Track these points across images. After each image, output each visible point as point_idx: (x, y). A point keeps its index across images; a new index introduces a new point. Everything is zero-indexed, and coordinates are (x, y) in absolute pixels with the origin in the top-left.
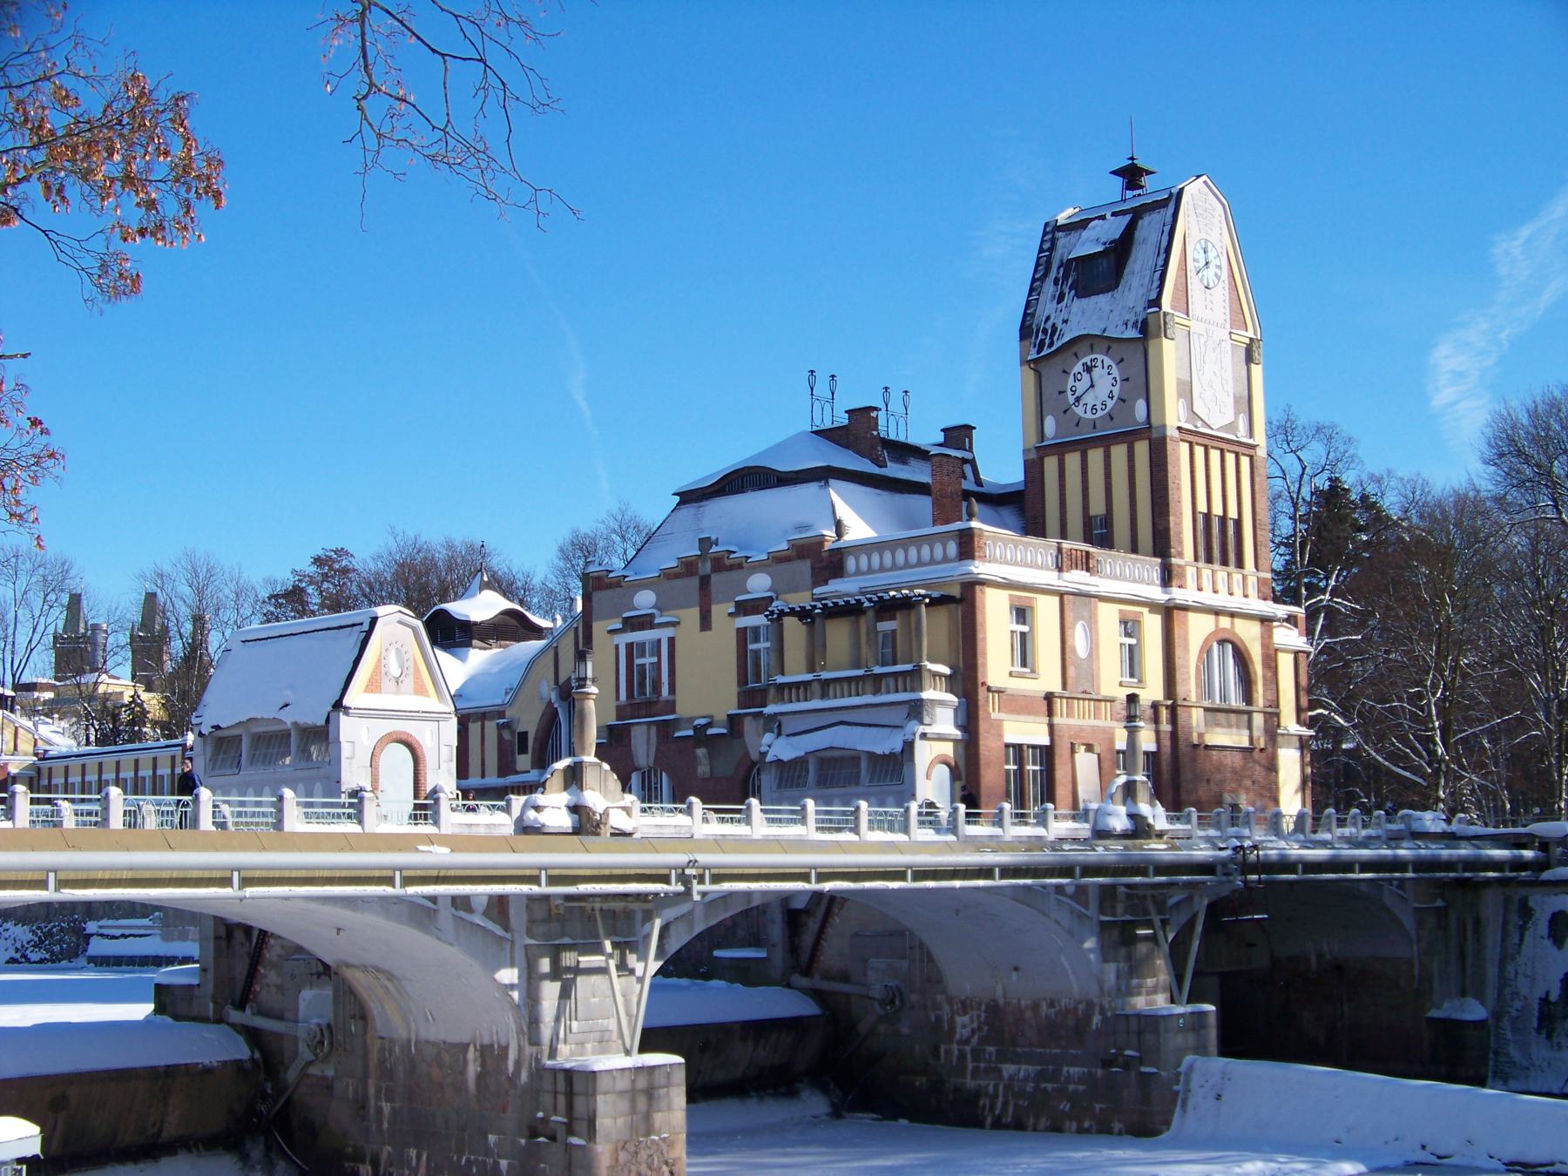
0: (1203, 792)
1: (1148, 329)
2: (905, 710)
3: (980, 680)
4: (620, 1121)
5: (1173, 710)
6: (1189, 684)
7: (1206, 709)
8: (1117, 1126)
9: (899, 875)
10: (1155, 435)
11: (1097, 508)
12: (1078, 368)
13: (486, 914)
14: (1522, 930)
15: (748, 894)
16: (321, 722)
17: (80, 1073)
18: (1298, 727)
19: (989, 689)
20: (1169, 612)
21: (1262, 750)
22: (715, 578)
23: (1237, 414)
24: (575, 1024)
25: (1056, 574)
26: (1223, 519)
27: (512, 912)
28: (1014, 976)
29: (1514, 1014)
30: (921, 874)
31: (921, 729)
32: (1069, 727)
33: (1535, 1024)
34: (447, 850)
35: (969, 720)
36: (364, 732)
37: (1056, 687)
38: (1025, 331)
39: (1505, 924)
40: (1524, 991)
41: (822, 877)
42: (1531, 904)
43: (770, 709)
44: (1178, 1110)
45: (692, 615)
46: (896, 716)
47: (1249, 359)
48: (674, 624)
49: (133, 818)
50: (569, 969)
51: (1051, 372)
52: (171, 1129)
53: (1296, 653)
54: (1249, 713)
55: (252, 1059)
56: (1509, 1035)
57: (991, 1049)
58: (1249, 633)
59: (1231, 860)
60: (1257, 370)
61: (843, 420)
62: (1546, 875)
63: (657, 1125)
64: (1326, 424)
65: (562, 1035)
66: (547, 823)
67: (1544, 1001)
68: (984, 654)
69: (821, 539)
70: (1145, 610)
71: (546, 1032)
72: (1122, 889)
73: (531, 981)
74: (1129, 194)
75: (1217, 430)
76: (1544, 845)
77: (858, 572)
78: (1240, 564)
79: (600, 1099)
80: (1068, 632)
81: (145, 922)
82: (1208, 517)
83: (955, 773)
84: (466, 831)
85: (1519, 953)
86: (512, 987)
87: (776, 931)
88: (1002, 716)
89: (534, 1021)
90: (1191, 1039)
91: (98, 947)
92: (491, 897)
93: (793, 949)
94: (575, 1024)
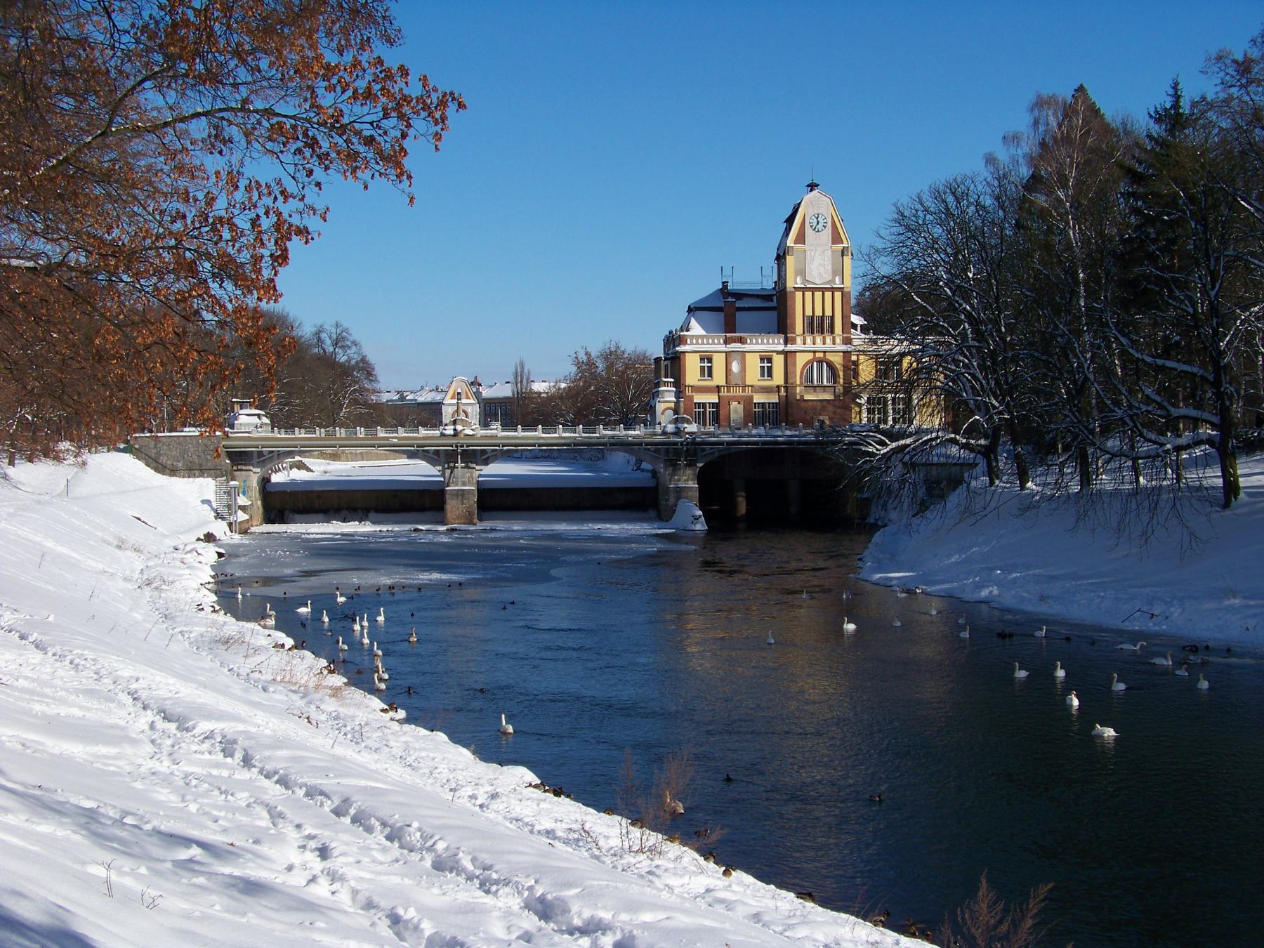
5: (786, 387)
13: (433, 454)
17: (424, 491)
35: (679, 394)
60: (847, 260)
70: (774, 354)
78: (832, 332)
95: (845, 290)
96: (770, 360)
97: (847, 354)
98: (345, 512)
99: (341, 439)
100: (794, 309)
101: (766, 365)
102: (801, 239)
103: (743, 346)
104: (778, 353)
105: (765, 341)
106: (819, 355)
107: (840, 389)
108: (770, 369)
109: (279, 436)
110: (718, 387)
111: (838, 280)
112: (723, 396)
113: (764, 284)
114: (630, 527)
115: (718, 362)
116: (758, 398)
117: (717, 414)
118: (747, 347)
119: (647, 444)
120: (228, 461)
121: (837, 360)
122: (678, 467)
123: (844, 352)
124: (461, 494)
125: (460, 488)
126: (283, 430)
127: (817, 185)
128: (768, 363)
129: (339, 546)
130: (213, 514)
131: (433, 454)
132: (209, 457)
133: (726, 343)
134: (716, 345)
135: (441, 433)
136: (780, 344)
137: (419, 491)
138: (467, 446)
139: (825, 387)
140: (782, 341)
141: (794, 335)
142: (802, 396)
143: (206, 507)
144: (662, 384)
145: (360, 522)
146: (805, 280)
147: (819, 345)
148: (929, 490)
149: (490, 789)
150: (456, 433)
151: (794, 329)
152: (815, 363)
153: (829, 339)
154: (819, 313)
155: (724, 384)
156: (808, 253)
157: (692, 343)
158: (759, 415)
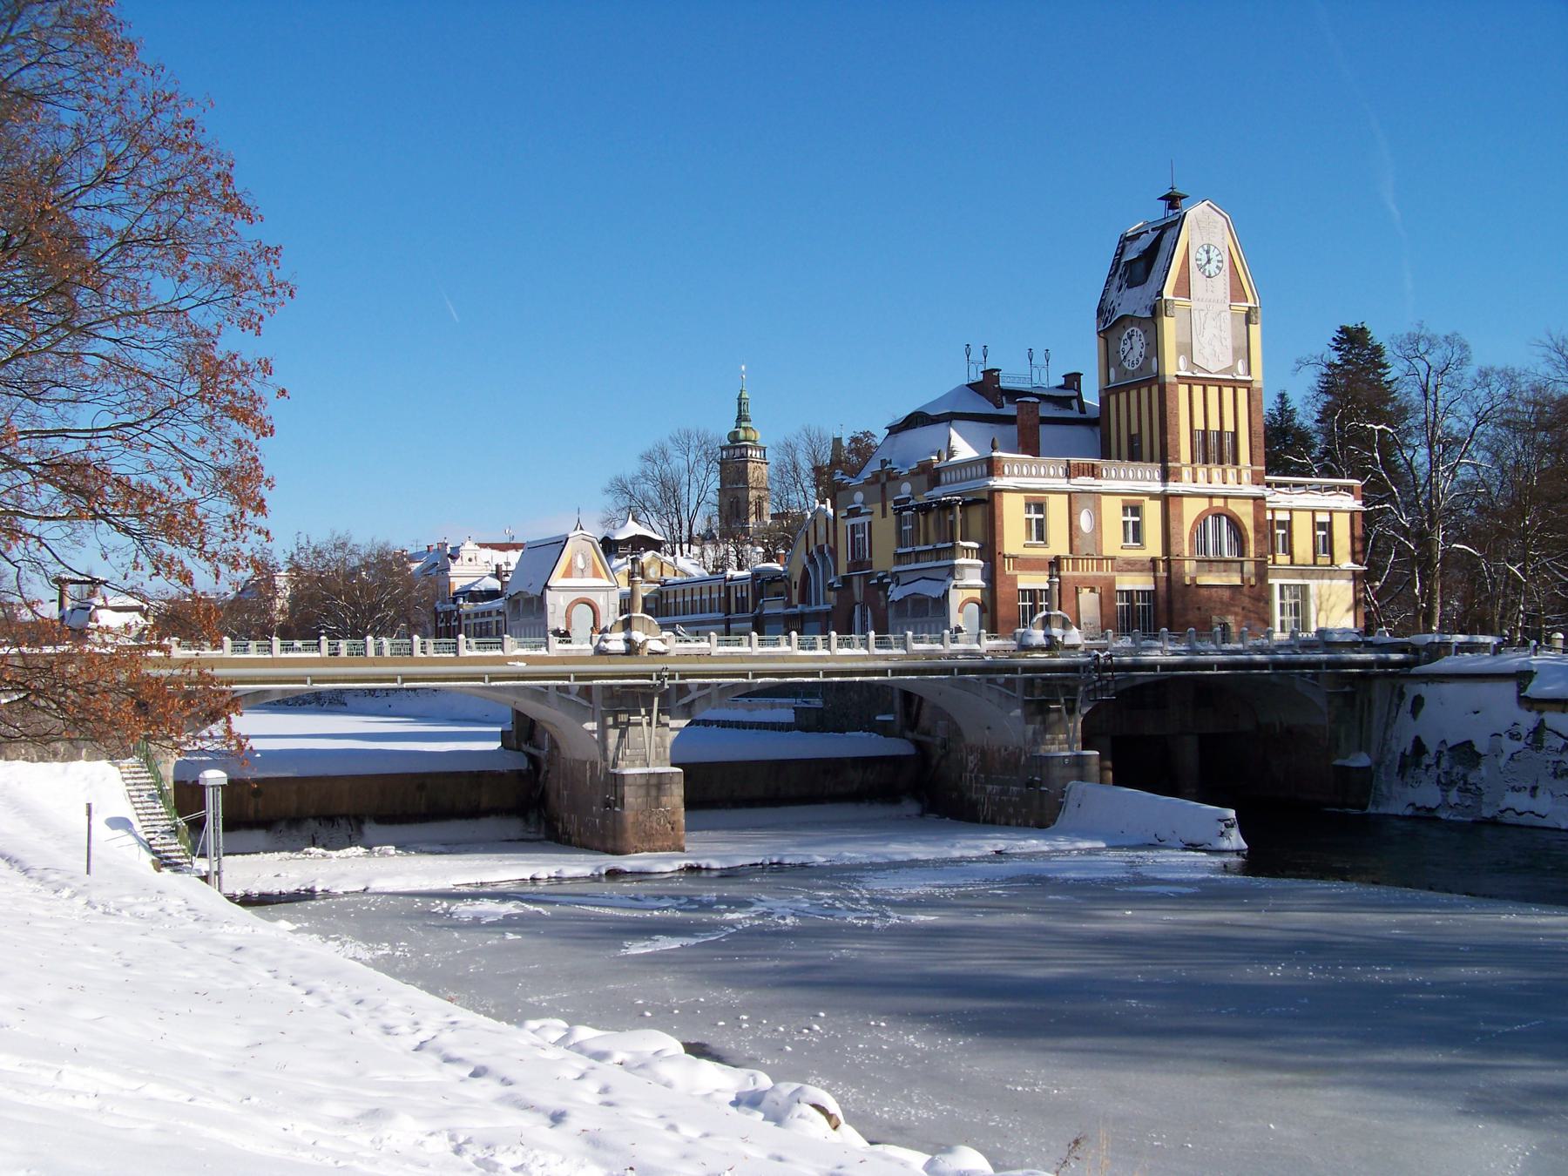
0: (1192, 616)
1: (1157, 311)
2: (947, 571)
4: (639, 800)
5: (1168, 563)
7: (1197, 561)
8: (1032, 822)
9: (815, 674)
10: (1160, 381)
11: (1134, 430)
12: (1125, 336)
13: (578, 695)
14: (1398, 706)
16: (539, 594)
18: (1352, 564)
19: (1004, 556)
21: (1251, 586)
22: (888, 485)
23: (1235, 361)
24: (628, 751)
25: (1066, 480)
26: (1221, 433)
28: (987, 732)
29: (1388, 763)
30: (828, 674)
31: (954, 582)
32: (1074, 577)
33: (1397, 770)
34: (524, 664)
35: (991, 575)
36: (562, 598)
37: (1063, 550)
38: (1100, 312)
39: (1391, 702)
40: (1394, 748)
41: (756, 676)
42: (1405, 690)
44: (1061, 813)
45: (878, 507)
46: (942, 574)
47: (1248, 321)
48: (871, 513)
49: (379, 651)
50: (623, 723)
51: (1112, 336)
52: (485, 802)
53: (1352, 513)
54: (1242, 562)
55: (528, 770)
56: (1383, 777)
57: (982, 776)
58: (1245, 512)
59: (1090, 663)
60: (1255, 330)
61: (981, 377)
62: (1415, 670)
63: (663, 803)
64: (411, 551)
65: (620, 756)
66: (610, 648)
67: (1403, 754)
69: (931, 462)
70: (1146, 499)
71: (611, 755)
72: (1039, 680)
73: (603, 729)
74: (1171, 212)
75: (1216, 373)
76: (1416, 649)
77: (947, 483)
78: (1236, 462)
80: (1074, 517)
82: (1205, 432)
83: (983, 608)
84: (565, 654)
85: (1395, 722)
86: (593, 732)
87: (897, 704)
88: (1017, 572)
89: (605, 749)
90: (1074, 772)
92: (581, 686)
93: (907, 714)
94: (628, 751)
95: (1255, 385)
96: (1136, 510)
98: (313, 825)
99: (421, 662)
100: (1177, 415)
101: (1130, 519)
102: (1184, 288)
103: (1097, 482)
104: (1153, 496)
106: (1218, 503)
107: (1249, 567)
111: (1241, 367)
112: (1067, 578)
113: (1036, 380)
115: (1057, 508)
118: (1104, 485)
119: (1026, 669)
122: (1053, 717)
123: (1255, 499)
124: (656, 784)
129: (1196, 931)
131: (578, 695)
133: (1068, 475)
139: (1226, 561)
141: (1178, 465)
142: (1193, 579)
144: (959, 550)
146: (1192, 364)
147: (1217, 486)
150: (632, 649)
151: (1178, 452)
156: (1195, 315)
157: (1011, 475)
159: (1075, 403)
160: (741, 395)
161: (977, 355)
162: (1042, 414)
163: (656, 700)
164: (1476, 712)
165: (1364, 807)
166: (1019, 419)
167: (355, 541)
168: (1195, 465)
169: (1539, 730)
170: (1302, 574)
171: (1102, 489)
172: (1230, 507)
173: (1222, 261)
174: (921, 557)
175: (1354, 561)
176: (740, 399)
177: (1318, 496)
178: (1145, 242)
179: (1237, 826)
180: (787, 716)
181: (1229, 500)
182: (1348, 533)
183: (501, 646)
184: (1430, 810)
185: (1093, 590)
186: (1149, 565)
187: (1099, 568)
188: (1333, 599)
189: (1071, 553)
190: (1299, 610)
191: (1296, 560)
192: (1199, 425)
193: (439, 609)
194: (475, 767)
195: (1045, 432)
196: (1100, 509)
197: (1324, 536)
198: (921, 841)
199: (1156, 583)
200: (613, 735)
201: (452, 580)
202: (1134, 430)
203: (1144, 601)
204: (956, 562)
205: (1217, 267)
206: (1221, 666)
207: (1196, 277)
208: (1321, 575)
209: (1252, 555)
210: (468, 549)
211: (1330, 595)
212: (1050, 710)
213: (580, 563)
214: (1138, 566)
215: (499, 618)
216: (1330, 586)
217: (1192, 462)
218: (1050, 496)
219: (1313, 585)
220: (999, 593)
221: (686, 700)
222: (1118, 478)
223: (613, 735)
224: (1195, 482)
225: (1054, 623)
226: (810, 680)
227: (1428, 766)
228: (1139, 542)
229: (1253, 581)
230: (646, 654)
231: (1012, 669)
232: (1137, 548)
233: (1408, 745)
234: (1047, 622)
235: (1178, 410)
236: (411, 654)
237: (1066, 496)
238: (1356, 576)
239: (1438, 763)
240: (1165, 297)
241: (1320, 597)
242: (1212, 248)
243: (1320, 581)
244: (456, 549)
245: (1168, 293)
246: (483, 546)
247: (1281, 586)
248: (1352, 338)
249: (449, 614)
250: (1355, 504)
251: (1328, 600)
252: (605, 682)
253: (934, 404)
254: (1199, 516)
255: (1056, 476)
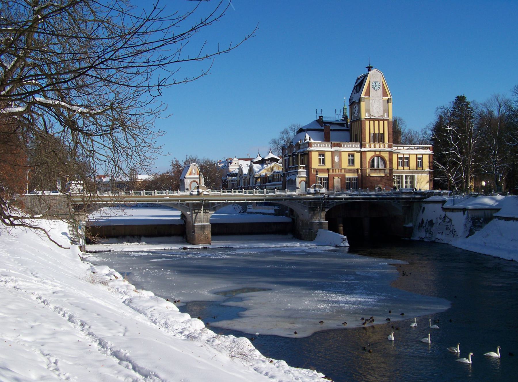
3: (310, 167)
5: (361, 170)
6: (366, 165)
11: (356, 134)
13: (186, 205)
15: (145, 203)
17: (171, 225)
19: (312, 169)
20: (361, 152)
23: (384, 114)
26: (379, 134)
27: (190, 205)
30: (248, 200)
31: (298, 176)
32: (333, 174)
35: (308, 173)
36: (188, 181)
38: (350, 100)
41: (228, 201)
43: (288, 172)
47: (388, 102)
50: (196, 212)
53: (430, 155)
54: (385, 170)
60: (390, 105)
67: (419, 223)
68: (311, 163)
70: (355, 152)
71: (194, 220)
75: (378, 117)
78: (384, 142)
79: (196, 228)
80: (333, 158)
81: (251, 206)
86: (190, 214)
91: (248, 210)
94: (198, 219)
95: (390, 120)
96: (353, 156)
97: (390, 153)
98: (128, 237)
100: (365, 129)
101: (351, 158)
102: (368, 93)
103: (340, 148)
105: (351, 146)
107: (387, 171)
108: (353, 160)
109: (245, 195)
110: (328, 170)
111: (386, 115)
113: (337, 118)
114: (309, 245)
115: (328, 156)
116: (348, 175)
117: (327, 182)
118: (342, 149)
119: (304, 199)
120: (73, 210)
121: (386, 156)
122: (316, 212)
123: (389, 152)
124: (203, 227)
125: (202, 224)
126: (247, 191)
127: (372, 67)
128: (352, 157)
130: (69, 241)
131: (186, 205)
132: (62, 207)
134: (326, 147)
135: (190, 194)
136: (358, 147)
137: (169, 225)
138: (208, 201)
140: (359, 146)
141: (365, 143)
142: (369, 175)
143: (65, 237)
145: (139, 243)
147: (377, 149)
148: (474, 224)
149: (79, 321)
150: (199, 194)
152: (375, 157)
153: (382, 145)
154: (377, 132)
155: (331, 167)
156: (371, 101)
157: (314, 146)
158: (348, 184)
159: (345, 125)
160: (344, 107)
161: (319, 112)
162: (331, 128)
163: (203, 206)
164: (434, 212)
165: (410, 238)
166: (324, 130)
167: (199, 158)
168: (370, 143)
169: (445, 217)
170: (412, 172)
171: (341, 150)
172: (381, 154)
173: (380, 86)
174: (293, 169)
175: (430, 169)
176: (344, 108)
177: (418, 150)
178: (361, 79)
179: (347, 240)
180: (273, 211)
181: (381, 153)
182: (428, 160)
183: (285, 192)
184: (423, 239)
185: (338, 178)
186: (356, 171)
187: (341, 172)
188: (422, 180)
189: (332, 167)
190: (412, 182)
191: (411, 168)
192: (372, 132)
193: (223, 179)
194: (167, 223)
195: (332, 133)
196: (341, 156)
197: (420, 162)
198: (264, 243)
199: (358, 176)
200: (194, 215)
201: (230, 170)
202: (356, 134)
203: (355, 181)
204: (298, 170)
205: (379, 87)
206: (363, 199)
207: (371, 90)
208: (419, 173)
209: (388, 168)
210: (235, 160)
211: (421, 179)
212: (315, 210)
213: (194, 171)
214: (352, 171)
215: (236, 182)
216: (421, 176)
217: (370, 142)
218: (326, 152)
219: (416, 176)
220: (310, 179)
221: (214, 207)
222: (347, 147)
223: (194, 215)
224: (370, 147)
225: (317, 187)
226: (243, 202)
227: (424, 226)
228: (354, 164)
229: (388, 175)
230: (202, 195)
231: (300, 199)
232: (352, 166)
233: (421, 221)
234: (315, 187)
235: (365, 128)
236: (151, 195)
237: (331, 152)
238: (430, 173)
239: (426, 226)
240: (362, 96)
241: (418, 179)
242: (377, 82)
243: (418, 174)
244: (231, 160)
245: (363, 95)
246: (239, 159)
247: (406, 176)
248: (460, 99)
249: (225, 180)
250: (431, 152)
251: (420, 180)
252: (218, 202)
253: (305, 126)
254: (372, 157)
255: (328, 147)
